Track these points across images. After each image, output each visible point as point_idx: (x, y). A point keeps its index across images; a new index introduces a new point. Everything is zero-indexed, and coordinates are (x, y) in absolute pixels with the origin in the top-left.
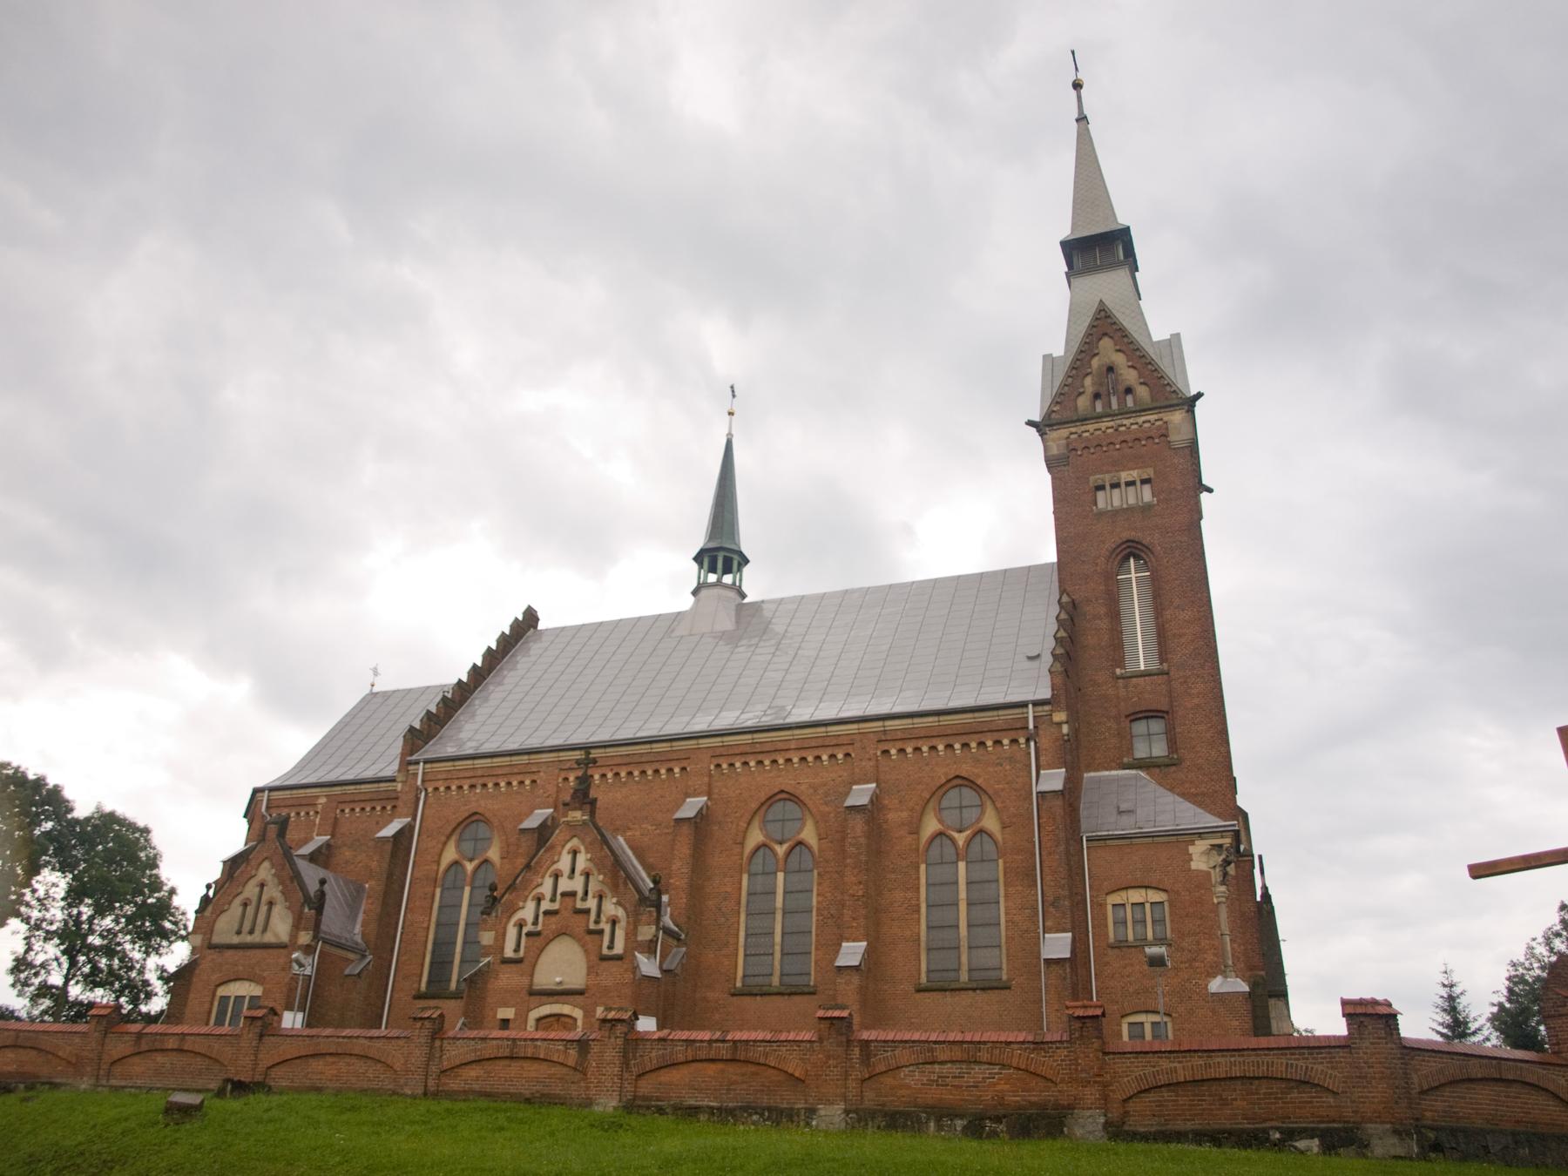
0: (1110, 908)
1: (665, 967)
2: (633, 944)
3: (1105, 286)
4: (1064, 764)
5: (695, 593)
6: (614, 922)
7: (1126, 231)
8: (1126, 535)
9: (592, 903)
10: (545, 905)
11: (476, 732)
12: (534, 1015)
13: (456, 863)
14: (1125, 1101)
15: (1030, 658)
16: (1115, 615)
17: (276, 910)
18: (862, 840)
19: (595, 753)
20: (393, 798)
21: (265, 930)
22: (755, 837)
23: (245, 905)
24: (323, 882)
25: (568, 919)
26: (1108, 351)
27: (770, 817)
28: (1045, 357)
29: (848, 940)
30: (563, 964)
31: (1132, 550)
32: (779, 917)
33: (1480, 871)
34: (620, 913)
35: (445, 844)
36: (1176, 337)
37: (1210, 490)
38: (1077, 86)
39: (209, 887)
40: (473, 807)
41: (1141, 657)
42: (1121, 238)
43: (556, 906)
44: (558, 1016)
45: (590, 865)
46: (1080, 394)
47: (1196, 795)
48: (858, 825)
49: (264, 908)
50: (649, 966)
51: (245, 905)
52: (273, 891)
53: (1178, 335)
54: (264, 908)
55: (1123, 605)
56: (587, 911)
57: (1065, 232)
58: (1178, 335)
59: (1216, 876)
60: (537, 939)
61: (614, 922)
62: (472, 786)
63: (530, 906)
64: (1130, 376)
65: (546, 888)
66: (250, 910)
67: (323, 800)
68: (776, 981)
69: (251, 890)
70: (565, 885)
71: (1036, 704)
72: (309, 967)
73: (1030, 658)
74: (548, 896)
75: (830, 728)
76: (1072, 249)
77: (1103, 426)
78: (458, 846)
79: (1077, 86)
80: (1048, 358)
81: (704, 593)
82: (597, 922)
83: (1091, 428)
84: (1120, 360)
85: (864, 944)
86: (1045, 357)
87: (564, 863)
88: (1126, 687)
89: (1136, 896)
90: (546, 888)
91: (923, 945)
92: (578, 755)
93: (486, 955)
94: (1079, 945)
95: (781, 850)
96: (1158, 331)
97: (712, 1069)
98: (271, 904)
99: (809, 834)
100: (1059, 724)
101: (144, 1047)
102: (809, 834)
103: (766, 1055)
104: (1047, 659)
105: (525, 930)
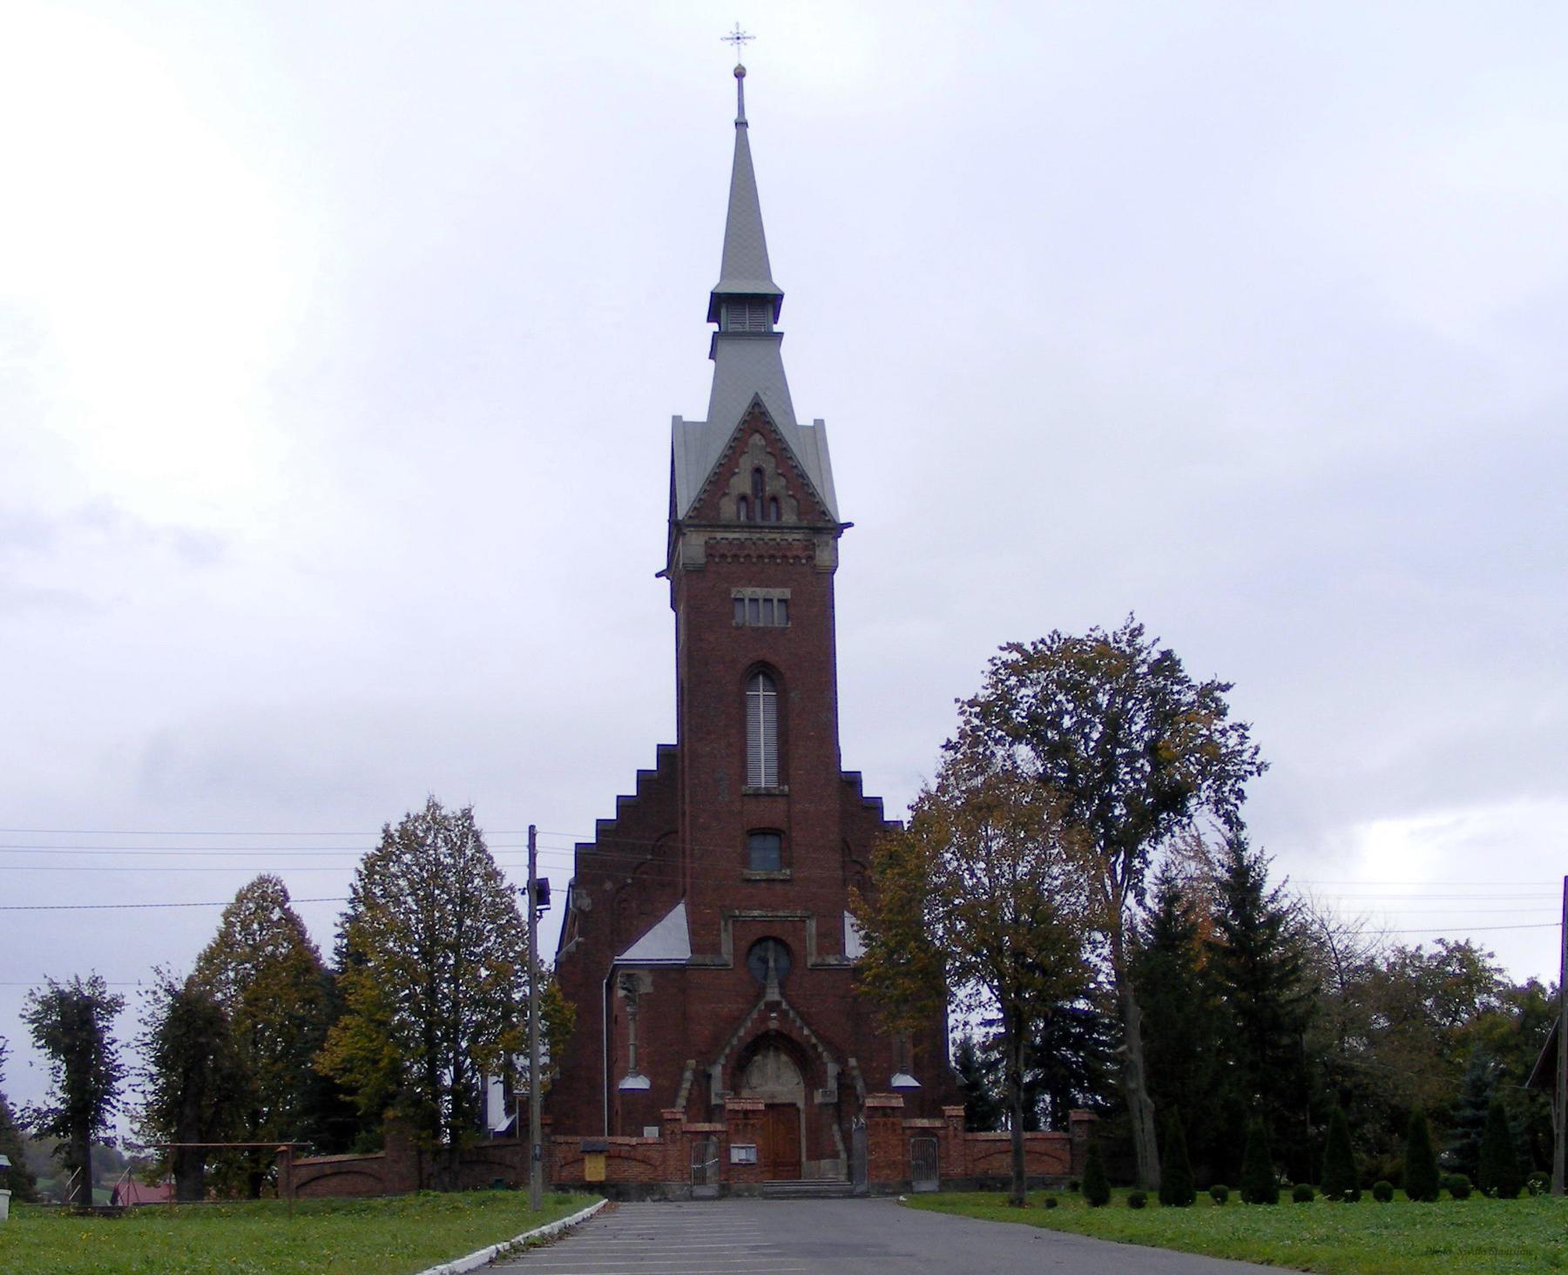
28: (674, 417)
31: (765, 670)
33: (532, 828)
36: (819, 424)
38: (740, 74)
41: (763, 773)
46: (725, 494)
53: (822, 421)
58: (822, 421)
76: (720, 304)
79: (740, 74)
80: (680, 427)
85: (680, 909)
86: (674, 417)
96: (804, 418)
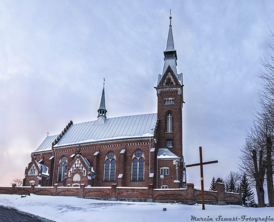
0: (160, 170)
1: (92, 178)
2: (87, 175)
3: (171, 62)
4: (155, 147)
5: (98, 117)
6: (84, 171)
7: (175, 51)
8: (169, 109)
9: (81, 168)
10: (74, 169)
11: (63, 143)
12: (73, 185)
13: (61, 163)
14: (155, 197)
15: (152, 130)
16: (166, 123)
17: (36, 170)
18: (123, 159)
19: (81, 145)
20: (51, 153)
21: (34, 173)
22: (106, 158)
23: (31, 170)
24: (42, 166)
25: (77, 171)
26: (170, 75)
27: (109, 155)
29: (120, 174)
30: (77, 178)
32: (110, 170)
34: (85, 170)
35: (59, 160)
37: (185, 103)
38: (171, 18)
39: (26, 168)
40: (63, 154)
42: (175, 52)
43: (76, 169)
44: (77, 185)
45: (81, 163)
47: (176, 153)
48: (122, 156)
49: (34, 170)
50: (89, 178)
51: (31, 170)
52: (35, 168)
54: (34, 170)
55: (168, 121)
56: (80, 170)
57: (165, 50)
59: (177, 165)
60: (73, 174)
61: (84, 171)
62: (63, 151)
63: (72, 169)
64: (173, 80)
65: (74, 166)
66: (32, 171)
67: (41, 154)
68: (109, 180)
69: (32, 168)
70: (77, 166)
71: (151, 137)
72: (40, 179)
73: (152, 130)
74: (74, 167)
75: (118, 140)
77: (167, 89)
78: (61, 160)
81: (99, 117)
82: (82, 171)
83: (165, 89)
84: (171, 77)
87: (77, 162)
88: (166, 135)
89: (164, 168)
90: (74, 166)
91: (132, 175)
92: (79, 145)
93: (65, 176)
94: (155, 175)
95: (110, 160)
97: (96, 192)
98: (35, 170)
99: (115, 157)
100: (155, 141)
101: (19, 189)
102: (115, 157)
103: (104, 190)
104: (154, 130)
105: (71, 172)
